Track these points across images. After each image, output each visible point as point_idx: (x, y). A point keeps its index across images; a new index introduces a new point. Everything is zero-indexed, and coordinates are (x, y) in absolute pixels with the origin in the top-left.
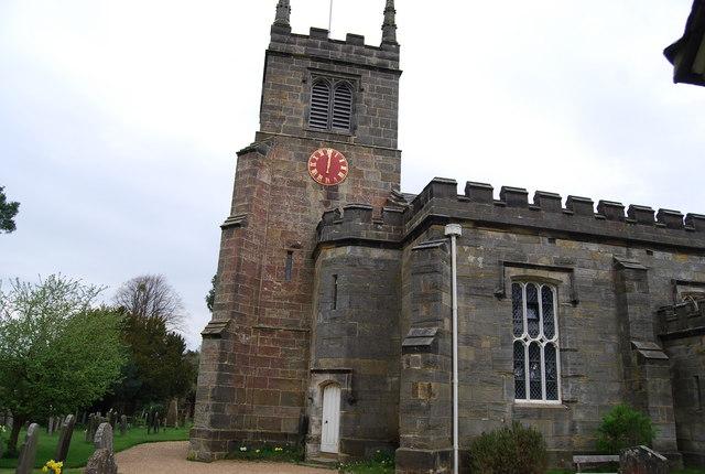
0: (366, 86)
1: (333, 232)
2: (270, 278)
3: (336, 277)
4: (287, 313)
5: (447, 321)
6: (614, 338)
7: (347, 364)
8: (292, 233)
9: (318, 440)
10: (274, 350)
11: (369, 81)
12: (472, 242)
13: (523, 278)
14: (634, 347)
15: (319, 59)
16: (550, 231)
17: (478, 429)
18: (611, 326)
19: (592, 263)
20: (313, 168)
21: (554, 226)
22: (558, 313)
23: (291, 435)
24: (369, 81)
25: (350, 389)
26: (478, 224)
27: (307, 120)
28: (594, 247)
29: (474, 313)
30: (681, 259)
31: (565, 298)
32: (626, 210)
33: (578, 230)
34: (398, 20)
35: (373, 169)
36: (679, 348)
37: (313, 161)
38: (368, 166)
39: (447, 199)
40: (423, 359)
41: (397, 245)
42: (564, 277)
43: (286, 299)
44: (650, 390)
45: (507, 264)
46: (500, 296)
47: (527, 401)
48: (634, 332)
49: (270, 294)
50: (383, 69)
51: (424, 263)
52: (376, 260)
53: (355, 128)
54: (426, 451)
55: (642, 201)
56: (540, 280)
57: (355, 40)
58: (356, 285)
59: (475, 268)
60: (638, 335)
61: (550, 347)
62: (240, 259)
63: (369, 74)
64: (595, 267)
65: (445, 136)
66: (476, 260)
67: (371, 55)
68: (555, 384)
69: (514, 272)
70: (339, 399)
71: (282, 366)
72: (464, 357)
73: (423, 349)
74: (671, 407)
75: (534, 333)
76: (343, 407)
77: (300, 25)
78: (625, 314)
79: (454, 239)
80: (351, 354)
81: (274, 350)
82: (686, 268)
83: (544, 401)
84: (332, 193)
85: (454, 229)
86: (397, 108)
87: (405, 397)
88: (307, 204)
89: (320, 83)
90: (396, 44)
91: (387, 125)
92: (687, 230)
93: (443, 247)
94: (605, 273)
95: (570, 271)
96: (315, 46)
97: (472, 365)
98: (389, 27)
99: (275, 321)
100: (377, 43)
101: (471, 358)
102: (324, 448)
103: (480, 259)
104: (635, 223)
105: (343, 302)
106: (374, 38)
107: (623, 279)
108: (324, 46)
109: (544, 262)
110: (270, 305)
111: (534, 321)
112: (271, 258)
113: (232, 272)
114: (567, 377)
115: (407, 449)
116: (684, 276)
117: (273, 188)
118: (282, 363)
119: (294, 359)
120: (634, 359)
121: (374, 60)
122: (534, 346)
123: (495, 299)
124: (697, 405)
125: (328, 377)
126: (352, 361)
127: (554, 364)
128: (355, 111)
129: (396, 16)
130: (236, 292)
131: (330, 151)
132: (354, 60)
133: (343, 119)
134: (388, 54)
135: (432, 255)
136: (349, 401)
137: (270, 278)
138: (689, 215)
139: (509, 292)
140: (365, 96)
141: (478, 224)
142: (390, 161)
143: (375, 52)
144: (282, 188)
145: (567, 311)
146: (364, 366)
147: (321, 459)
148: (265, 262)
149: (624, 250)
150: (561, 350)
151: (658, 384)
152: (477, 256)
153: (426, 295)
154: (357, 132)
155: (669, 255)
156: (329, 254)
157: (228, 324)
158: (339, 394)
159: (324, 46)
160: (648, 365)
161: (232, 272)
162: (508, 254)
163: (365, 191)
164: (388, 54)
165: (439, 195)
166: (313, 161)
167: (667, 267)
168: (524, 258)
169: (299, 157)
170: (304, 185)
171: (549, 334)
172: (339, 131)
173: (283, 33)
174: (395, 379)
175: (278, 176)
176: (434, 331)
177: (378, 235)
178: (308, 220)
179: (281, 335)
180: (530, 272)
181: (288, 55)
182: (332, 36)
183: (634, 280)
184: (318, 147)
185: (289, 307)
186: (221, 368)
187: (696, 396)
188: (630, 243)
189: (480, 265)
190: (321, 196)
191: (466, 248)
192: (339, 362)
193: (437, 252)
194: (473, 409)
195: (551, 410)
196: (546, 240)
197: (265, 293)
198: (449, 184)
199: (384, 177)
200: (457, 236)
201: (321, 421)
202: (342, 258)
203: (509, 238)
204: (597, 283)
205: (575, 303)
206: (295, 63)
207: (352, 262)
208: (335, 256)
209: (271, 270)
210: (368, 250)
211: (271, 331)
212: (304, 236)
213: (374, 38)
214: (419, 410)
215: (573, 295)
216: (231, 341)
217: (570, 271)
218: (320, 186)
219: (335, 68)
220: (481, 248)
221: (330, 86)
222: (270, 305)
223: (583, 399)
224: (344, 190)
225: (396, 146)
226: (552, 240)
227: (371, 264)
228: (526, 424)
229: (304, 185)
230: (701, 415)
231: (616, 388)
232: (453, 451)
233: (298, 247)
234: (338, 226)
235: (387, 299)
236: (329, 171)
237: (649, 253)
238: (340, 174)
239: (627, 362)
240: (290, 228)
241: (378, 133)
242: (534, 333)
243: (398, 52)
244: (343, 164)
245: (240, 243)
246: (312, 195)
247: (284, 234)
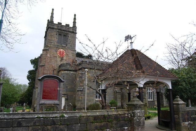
0: (69, 36)
1: (64, 68)
5: (85, 86)
11: (70, 35)
15: (59, 30)
17: (89, 104)
20: (58, 53)
24: (70, 35)
26: (91, 69)
27: (57, 43)
34: (77, 21)
37: (58, 52)
38: (69, 53)
39: (85, 64)
41: (76, 71)
44: (117, 97)
47: (149, 100)
50: (73, 32)
57: (67, 25)
63: (70, 33)
65: (84, 44)
67: (71, 29)
70: (64, 99)
73: (81, 91)
76: (65, 101)
77: (56, 21)
83: (151, 100)
84: (62, 59)
85: (87, 70)
86: (76, 41)
87: (77, 98)
89: (60, 35)
90: (76, 27)
93: (84, 73)
96: (59, 26)
98: (74, 23)
100: (72, 27)
101: (89, 92)
106: (71, 26)
108: (61, 27)
117: (50, 57)
121: (71, 30)
128: (67, 41)
129: (76, 20)
131: (62, 50)
132: (67, 30)
133: (65, 43)
134: (74, 29)
136: (66, 100)
140: (69, 38)
141: (91, 69)
143: (71, 29)
146: (69, 93)
151: (119, 96)
154: (67, 46)
156: (63, 72)
159: (61, 27)
164: (74, 29)
165: (84, 64)
166: (58, 52)
169: (55, 51)
170: (56, 57)
172: (64, 45)
173: (52, 23)
175: (51, 55)
176: (82, 88)
181: (53, 28)
182: (62, 24)
184: (59, 49)
190: (60, 59)
192: (65, 93)
193: (83, 74)
194: (89, 101)
202: (65, 73)
206: (55, 30)
207: (67, 74)
212: (56, 67)
213: (71, 26)
218: (59, 57)
219: (63, 32)
221: (60, 34)
224: (65, 58)
228: (97, 103)
229: (56, 57)
231: (113, 97)
233: (55, 70)
235: (73, 81)
236: (62, 54)
238: (64, 55)
239: (114, 92)
241: (72, 46)
243: (76, 28)
244: (65, 53)
245: (44, 69)
246: (58, 59)
247: (52, 67)
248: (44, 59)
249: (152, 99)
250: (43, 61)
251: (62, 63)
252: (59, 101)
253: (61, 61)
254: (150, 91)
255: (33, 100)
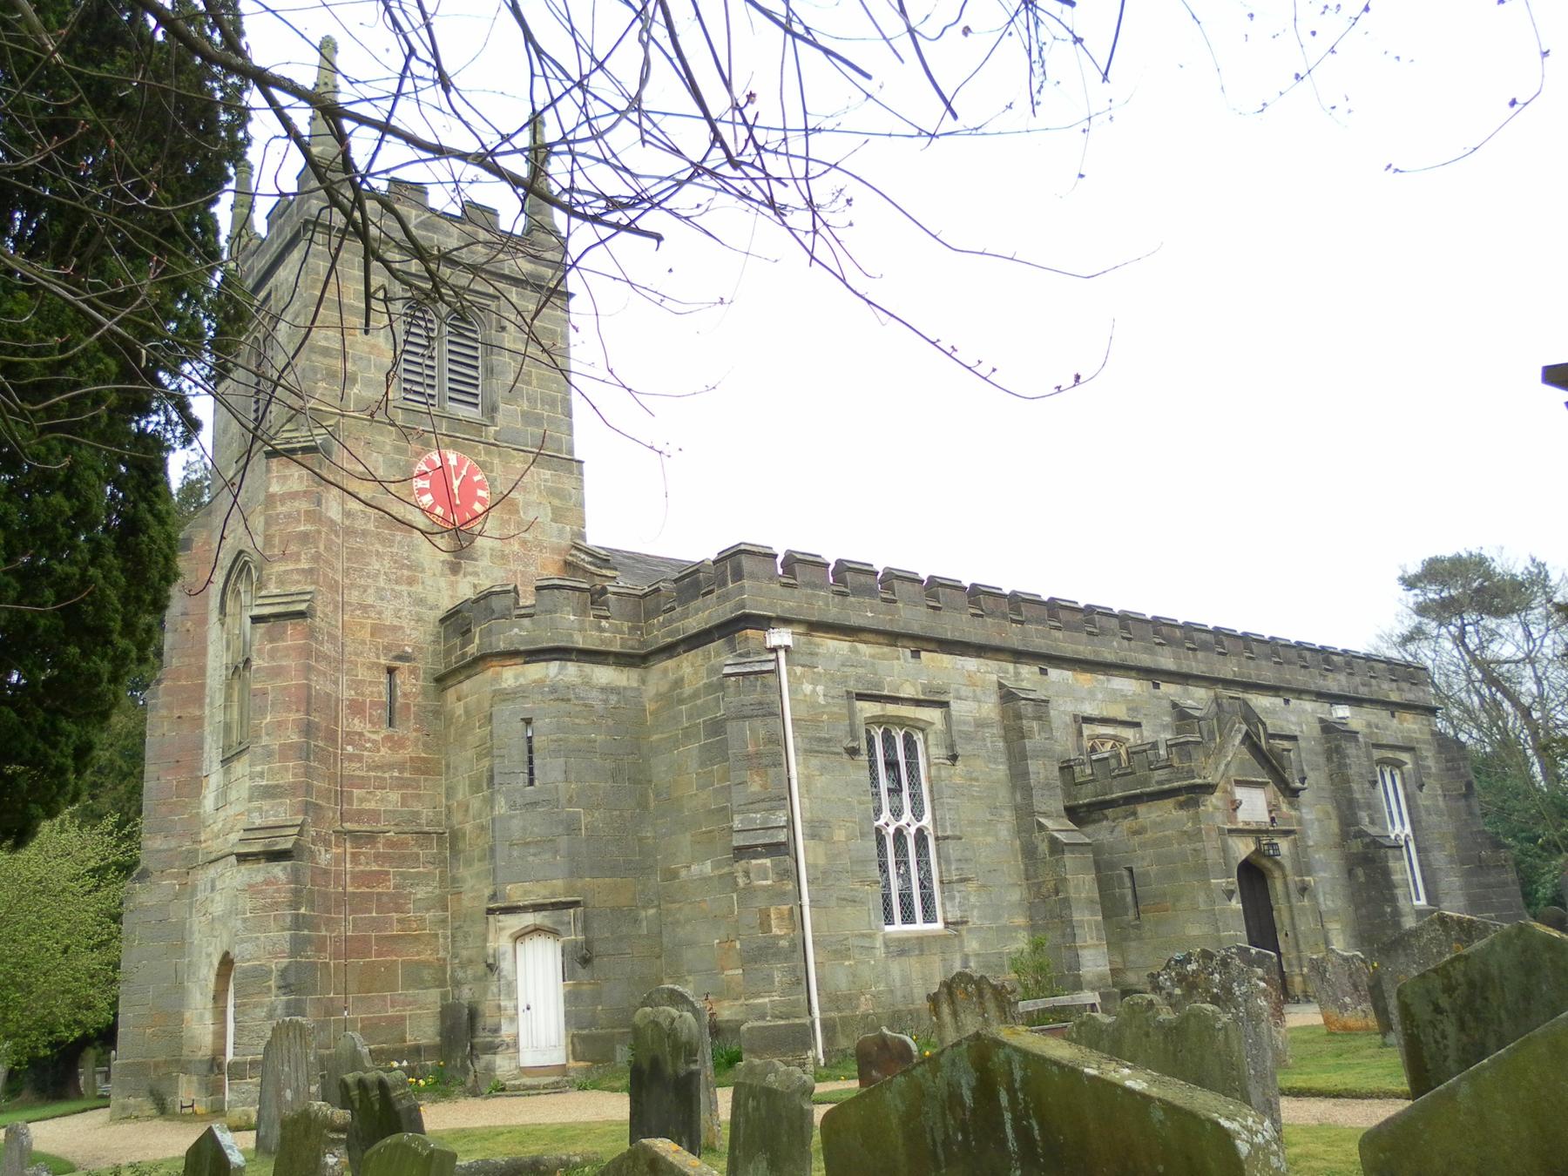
1: (517, 634)
2: (357, 725)
3: (528, 722)
4: (394, 796)
6: (1008, 815)
7: (570, 890)
8: (394, 629)
9: (515, 1044)
10: (381, 876)
12: (805, 659)
13: (876, 721)
14: (1041, 827)
16: (913, 637)
18: (1003, 795)
19: (972, 685)
20: (422, 492)
21: (916, 629)
22: (929, 778)
23: (427, 1048)
25: (581, 938)
26: (817, 626)
28: (971, 664)
29: (821, 781)
30: (1085, 680)
31: (938, 752)
32: (779, 560)
33: (949, 636)
35: (534, 497)
36: (1109, 832)
40: (774, 866)
42: (933, 715)
43: (391, 767)
45: (861, 697)
46: (853, 752)
47: (898, 928)
48: (1039, 803)
49: (360, 758)
51: (748, 699)
52: (603, 689)
53: (494, 409)
54: (797, 1021)
55: (805, 545)
56: (901, 722)
58: (573, 737)
59: (813, 705)
60: (1044, 808)
61: (921, 836)
62: (309, 687)
64: (976, 699)
66: (814, 691)
68: (931, 895)
69: (869, 709)
71: (399, 908)
72: (811, 861)
74: (1100, 918)
75: (897, 813)
78: (1025, 774)
79: (782, 654)
80: (575, 872)
81: (381, 876)
82: (1092, 694)
83: (919, 926)
85: (780, 637)
88: (415, 567)
91: (552, 403)
92: (885, 600)
94: (989, 708)
95: (944, 705)
97: (824, 873)
99: (374, 815)
102: (528, 1059)
103: (820, 689)
104: (1022, 623)
105: (550, 770)
107: (1019, 717)
109: (908, 691)
110: (362, 783)
111: (895, 791)
112: (356, 684)
113: (293, 716)
114: (950, 882)
115: (761, 1023)
116: (1089, 709)
118: (397, 902)
119: (421, 892)
120: (1044, 847)
122: (899, 834)
123: (846, 756)
124: (1131, 915)
125: (529, 919)
126: (579, 883)
127: (928, 863)
130: (308, 759)
133: (465, 389)
135: (764, 685)
136: (579, 960)
137: (357, 725)
138: (839, 562)
139: (864, 746)
142: (567, 483)
144: (364, 533)
145: (943, 773)
146: (598, 889)
147: (528, 1081)
148: (347, 694)
149: (1011, 667)
150: (937, 839)
151: (1082, 884)
152: (814, 683)
153: (758, 755)
154: (499, 417)
155: (1068, 675)
157: (302, 826)
158: (559, 946)
160: (1068, 856)
161: (293, 716)
162: (858, 679)
163: (524, 543)
167: (1074, 694)
168: (879, 685)
171: (918, 813)
174: (652, 911)
177: (602, 641)
178: (421, 602)
179: (390, 844)
180: (891, 709)
183: (1034, 718)
184: (427, 444)
185: (402, 784)
186: (298, 923)
187: (1129, 898)
188: (1018, 656)
189: (821, 700)
191: (799, 670)
192: (556, 888)
195: (935, 938)
196: (908, 652)
197: (351, 758)
198: (766, 555)
199: (558, 516)
200: (787, 648)
201: (516, 1008)
202: (540, 684)
203: (856, 651)
204: (981, 724)
205: (954, 758)
207: (559, 693)
208: (522, 681)
209: (356, 708)
210: (588, 668)
211: (371, 837)
212: (418, 634)
214: (774, 955)
215: (951, 746)
216: (304, 864)
217: (944, 705)
220: (820, 669)
222: (362, 783)
223: (975, 919)
225: (571, 452)
226: (916, 654)
227: (595, 698)
230: (1138, 927)
232: (813, 1023)
233: (403, 657)
234: (526, 621)
237: (1156, 686)
239: (1029, 852)
240: (389, 620)
241: (538, 420)
242: (897, 813)
244: (480, 485)
245: (306, 652)
247: (376, 630)
248: (293, 548)
249: (929, 916)
250: (279, 568)
251: (465, 589)
252: (994, 987)
253: (455, 569)
254: (907, 816)
255: (120, 1030)
